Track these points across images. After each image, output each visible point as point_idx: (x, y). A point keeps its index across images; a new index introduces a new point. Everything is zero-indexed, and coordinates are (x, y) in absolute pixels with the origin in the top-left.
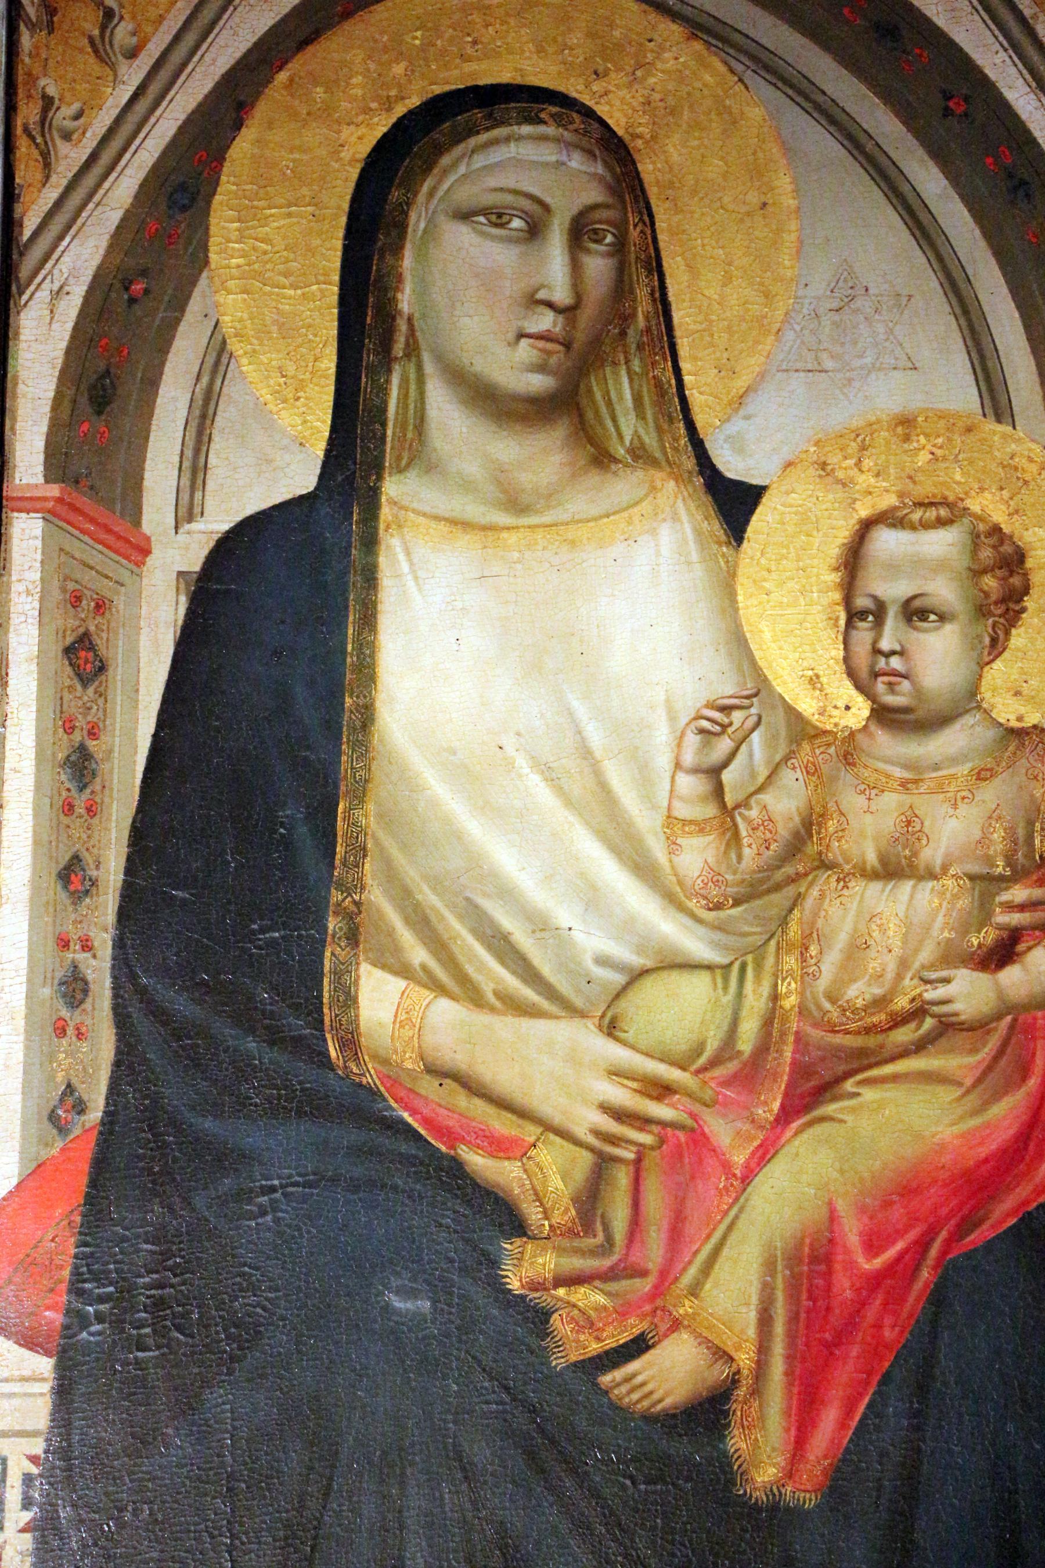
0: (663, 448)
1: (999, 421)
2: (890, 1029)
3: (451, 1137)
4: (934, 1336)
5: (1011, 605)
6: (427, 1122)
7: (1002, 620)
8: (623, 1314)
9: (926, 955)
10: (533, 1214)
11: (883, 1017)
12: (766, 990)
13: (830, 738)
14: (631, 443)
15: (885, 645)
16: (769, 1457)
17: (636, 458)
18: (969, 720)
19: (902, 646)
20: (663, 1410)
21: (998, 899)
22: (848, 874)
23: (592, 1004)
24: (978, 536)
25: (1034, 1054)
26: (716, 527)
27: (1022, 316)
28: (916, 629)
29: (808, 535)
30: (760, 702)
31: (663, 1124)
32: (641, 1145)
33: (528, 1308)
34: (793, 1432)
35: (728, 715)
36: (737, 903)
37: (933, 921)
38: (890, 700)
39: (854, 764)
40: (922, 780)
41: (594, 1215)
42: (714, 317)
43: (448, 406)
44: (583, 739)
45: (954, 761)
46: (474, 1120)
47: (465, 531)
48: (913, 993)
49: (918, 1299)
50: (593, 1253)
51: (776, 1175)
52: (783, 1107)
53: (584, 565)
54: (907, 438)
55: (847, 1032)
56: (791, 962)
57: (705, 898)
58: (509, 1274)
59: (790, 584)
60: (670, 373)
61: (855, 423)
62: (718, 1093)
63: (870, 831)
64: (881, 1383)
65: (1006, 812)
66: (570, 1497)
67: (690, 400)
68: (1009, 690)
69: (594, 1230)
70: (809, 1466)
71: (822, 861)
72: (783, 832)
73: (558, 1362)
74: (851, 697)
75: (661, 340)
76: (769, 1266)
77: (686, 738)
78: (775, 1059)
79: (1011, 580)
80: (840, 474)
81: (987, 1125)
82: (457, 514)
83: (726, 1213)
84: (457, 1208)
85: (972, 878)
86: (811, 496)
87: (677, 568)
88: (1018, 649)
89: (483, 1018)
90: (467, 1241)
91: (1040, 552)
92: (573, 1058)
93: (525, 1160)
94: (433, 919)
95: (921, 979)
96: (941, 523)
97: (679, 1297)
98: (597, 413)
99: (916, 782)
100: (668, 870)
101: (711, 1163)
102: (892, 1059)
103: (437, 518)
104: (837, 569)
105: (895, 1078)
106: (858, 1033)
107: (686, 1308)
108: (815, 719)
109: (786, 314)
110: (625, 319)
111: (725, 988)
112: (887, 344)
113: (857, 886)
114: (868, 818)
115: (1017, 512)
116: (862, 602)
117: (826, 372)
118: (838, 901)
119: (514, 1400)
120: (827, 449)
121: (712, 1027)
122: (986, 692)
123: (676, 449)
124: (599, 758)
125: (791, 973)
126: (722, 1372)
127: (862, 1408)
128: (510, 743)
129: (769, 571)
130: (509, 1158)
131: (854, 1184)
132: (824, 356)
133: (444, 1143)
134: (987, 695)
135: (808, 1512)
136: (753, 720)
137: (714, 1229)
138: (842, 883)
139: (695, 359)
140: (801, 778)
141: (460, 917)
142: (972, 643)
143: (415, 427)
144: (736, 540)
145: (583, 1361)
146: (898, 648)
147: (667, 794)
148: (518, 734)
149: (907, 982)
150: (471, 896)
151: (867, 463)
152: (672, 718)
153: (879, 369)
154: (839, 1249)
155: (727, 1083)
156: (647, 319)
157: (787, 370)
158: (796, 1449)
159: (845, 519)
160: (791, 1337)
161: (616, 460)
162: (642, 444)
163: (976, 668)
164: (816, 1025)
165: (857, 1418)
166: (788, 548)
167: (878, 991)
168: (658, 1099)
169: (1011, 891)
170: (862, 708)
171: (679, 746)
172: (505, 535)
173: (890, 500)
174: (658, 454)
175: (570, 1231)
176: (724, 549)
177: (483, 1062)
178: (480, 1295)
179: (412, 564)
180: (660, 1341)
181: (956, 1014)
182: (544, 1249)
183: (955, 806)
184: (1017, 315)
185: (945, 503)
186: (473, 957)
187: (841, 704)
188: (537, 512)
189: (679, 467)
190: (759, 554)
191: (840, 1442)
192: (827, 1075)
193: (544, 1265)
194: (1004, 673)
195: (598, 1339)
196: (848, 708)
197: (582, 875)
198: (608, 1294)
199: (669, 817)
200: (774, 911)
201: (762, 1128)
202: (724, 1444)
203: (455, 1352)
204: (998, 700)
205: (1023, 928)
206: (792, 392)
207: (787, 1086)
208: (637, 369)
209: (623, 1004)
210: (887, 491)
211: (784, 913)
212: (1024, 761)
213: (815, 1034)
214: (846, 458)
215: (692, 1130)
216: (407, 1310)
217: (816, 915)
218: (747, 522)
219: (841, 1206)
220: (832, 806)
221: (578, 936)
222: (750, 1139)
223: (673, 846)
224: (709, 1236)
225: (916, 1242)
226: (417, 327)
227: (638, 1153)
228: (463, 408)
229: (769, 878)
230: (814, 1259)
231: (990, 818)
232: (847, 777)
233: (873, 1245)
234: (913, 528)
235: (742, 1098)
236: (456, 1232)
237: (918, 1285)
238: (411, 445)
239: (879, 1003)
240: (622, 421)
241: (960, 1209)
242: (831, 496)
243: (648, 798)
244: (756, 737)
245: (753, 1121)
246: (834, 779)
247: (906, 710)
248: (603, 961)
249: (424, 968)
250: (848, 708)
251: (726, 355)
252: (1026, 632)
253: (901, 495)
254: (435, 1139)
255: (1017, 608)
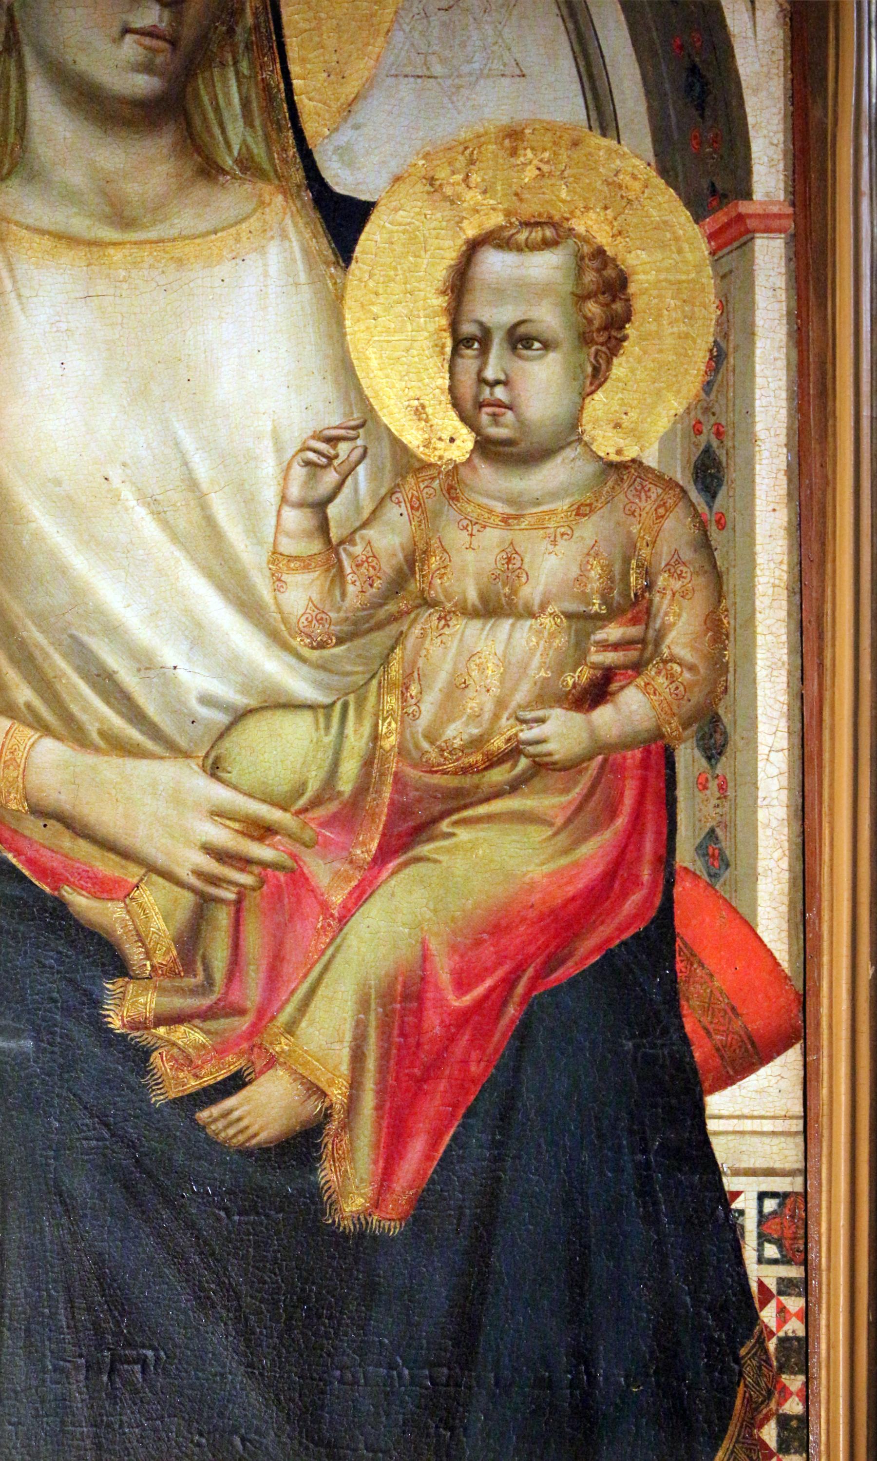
0: (271, 159)
1: (604, 135)
2: (486, 769)
3: (56, 879)
4: (517, 1070)
5: (614, 333)
6: (31, 862)
7: (604, 349)
8: (221, 1051)
9: (521, 696)
10: (135, 954)
11: (480, 757)
12: (366, 729)
13: (433, 472)
14: (239, 154)
15: (490, 374)
16: (357, 1187)
17: (244, 169)
18: (569, 453)
19: (506, 375)
20: (259, 1144)
21: (593, 638)
22: (449, 612)
23: (196, 744)
24: (582, 258)
25: (622, 794)
26: (324, 246)
27: (627, 18)
28: (520, 357)
29: (416, 256)
30: (368, 434)
31: (264, 865)
32: (242, 886)
33: (129, 1047)
34: (381, 1163)
35: (334, 447)
36: (340, 641)
37: (530, 659)
38: (494, 432)
39: (456, 499)
40: (522, 516)
41: (196, 953)
42: (323, 15)
43: (50, 108)
44: (190, 471)
45: (554, 496)
46: (78, 861)
47: (69, 247)
48: (509, 733)
49: (504, 1034)
50: (194, 992)
51: (371, 915)
52: (380, 847)
53: (192, 285)
54: (514, 153)
55: (445, 773)
56: (391, 702)
57: (309, 636)
58: (111, 1013)
59: (399, 309)
60: (278, 77)
61: (463, 135)
62: (318, 834)
63: (471, 569)
64: (465, 1116)
65: (602, 548)
66: (166, 1229)
67: (299, 106)
68: (609, 421)
69: (194, 970)
70: (395, 1196)
71: (425, 599)
72: (387, 568)
73: (157, 1099)
74: (455, 428)
75: (269, 39)
76: (364, 1004)
77: (292, 471)
78: (374, 799)
79: (614, 306)
80: (448, 191)
81: (575, 864)
82: (60, 228)
83: (323, 952)
84: (60, 948)
85: (569, 616)
86: (419, 214)
87: (284, 289)
88: (618, 380)
89: (89, 759)
90: (71, 981)
91: (641, 277)
92: (177, 799)
93: (128, 901)
94: (37, 654)
95: (517, 719)
96: (547, 244)
97: (276, 1035)
98: (205, 119)
99: (518, 517)
100: (273, 608)
101: (310, 906)
102: (487, 799)
103: (42, 232)
104: (444, 293)
105: (490, 818)
106: (455, 773)
107: (283, 1045)
108: (420, 452)
109: (396, 12)
110: (232, 14)
111: (328, 728)
112: (496, 48)
113: (458, 624)
114: (470, 556)
115: (620, 233)
116: (468, 329)
117: (436, 78)
118: (439, 640)
119: (113, 1136)
120: (435, 163)
121: (314, 767)
122: (587, 424)
123: (285, 161)
124: (205, 491)
125: (391, 713)
126: (315, 1107)
127: (447, 1139)
128: (116, 474)
129: (377, 294)
130: (112, 899)
131: (446, 923)
132: (433, 59)
133: (47, 884)
134: (588, 427)
135: (393, 1239)
136: (358, 453)
137: (311, 968)
138: (443, 622)
139: (303, 60)
140: (405, 513)
141: (65, 656)
142: (573, 372)
143: (17, 130)
144: (344, 261)
145: (182, 1097)
146: (502, 377)
147: (272, 530)
148: (124, 465)
149: (503, 722)
150: (76, 633)
151: (475, 178)
152: (279, 450)
153: (488, 76)
154: (431, 987)
155: (328, 823)
156: (255, 15)
157: (396, 76)
158: (383, 1180)
159: (453, 238)
160: (382, 1071)
161: (223, 172)
162: (251, 157)
163: (578, 400)
164: (415, 766)
165: (442, 1150)
166: (395, 269)
167: (475, 731)
168: (261, 839)
169: (606, 630)
170: (466, 440)
171: (285, 478)
172: (111, 251)
173: (497, 219)
174: (266, 166)
175: (172, 971)
176: (333, 270)
177: (87, 803)
178: (81, 1034)
179: (15, 282)
180: (256, 1078)
181: (550, 754)
182: (146, 989)
183: (554, 542)
184: (622, 17)
185: (550, 223)
186: (79, 697)
187: (446, 436)
188: (143, 227)
189: (287, 180)
190: (367, 276)
191: (425, 1173)
192: (422, 815)
193: (146, 1004)
194: (605, 404)
195: (196, 1076)
196: (452, 440)
197: (188, 612)
198: (207, 1032)
199: (274, 553)
200: (376, 651)
201: (360, 868)
202: (316, 1176)
203: (57, 1090)
204: (598, 433)
205: (618, 667)
206: (402, 99)
207: (385, 826)
208: (246, 72)
209: (227, 743)
210: (494, 209)
211: (386, 652)
212: (622, 496)
213: (413, 773)
214: (453, 173)
215: (293, 872)
216: (11, 1050)
217: (417, 654)
218: (355, 241)
219: (434, 945)
220: (435, 543)
221: (183, 675)
222: (348, 879)
223: (278, 583)
224: (305, 976)
225: (503, 980)
226: (17, 18)
227: (239, 893)
228: (66, 110)
229: (371, 616)
230: (406, 997)
231: (588, 554)
232: (450, 513)
233: (462, 985)
234: (520, 250)
235: (341, 839)
236: (59, 972)
237: (504, 1022)
238: (13, 150)
239: (477, 743)
240: (229, 128)
241: (547, 946)
242: (440, 215)
243: (253, 531)
244: (361, 469)
245: (351, 862)
246: (437, 514)
247: (508, 442)
248: (207, 700)
249: (28, 706)
250: (452, 440)
251: (335, 57)
252: (628, 362)
253: (508, 214)
254: (38, 879)
255: (619, 336)
